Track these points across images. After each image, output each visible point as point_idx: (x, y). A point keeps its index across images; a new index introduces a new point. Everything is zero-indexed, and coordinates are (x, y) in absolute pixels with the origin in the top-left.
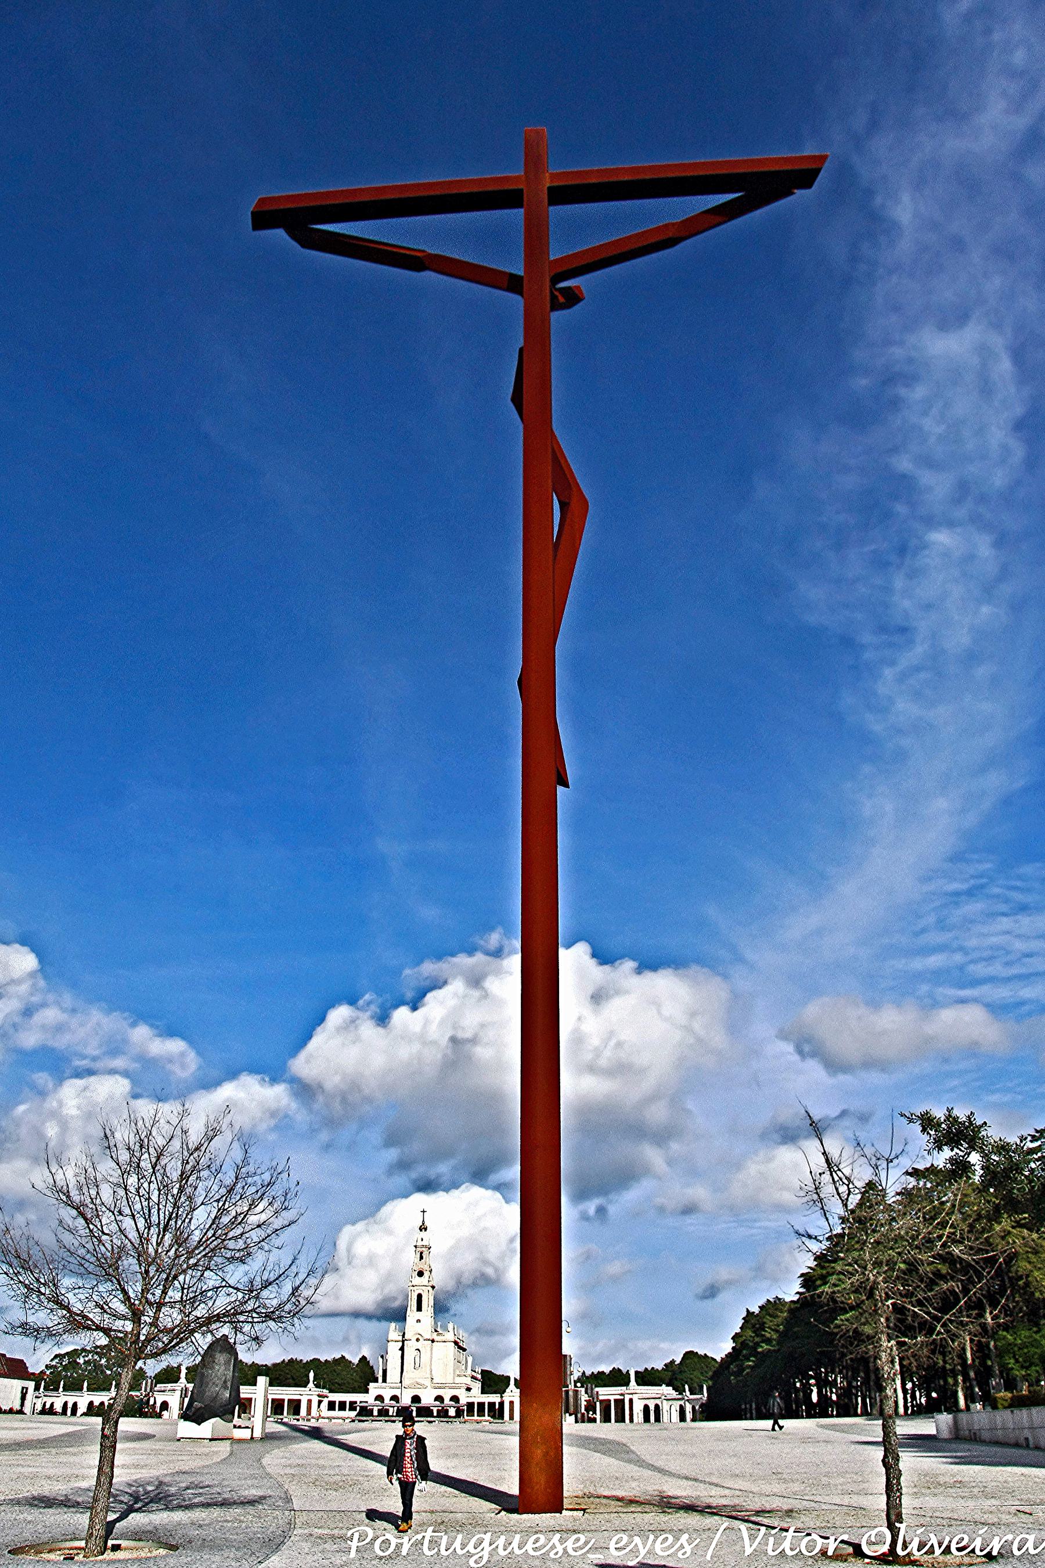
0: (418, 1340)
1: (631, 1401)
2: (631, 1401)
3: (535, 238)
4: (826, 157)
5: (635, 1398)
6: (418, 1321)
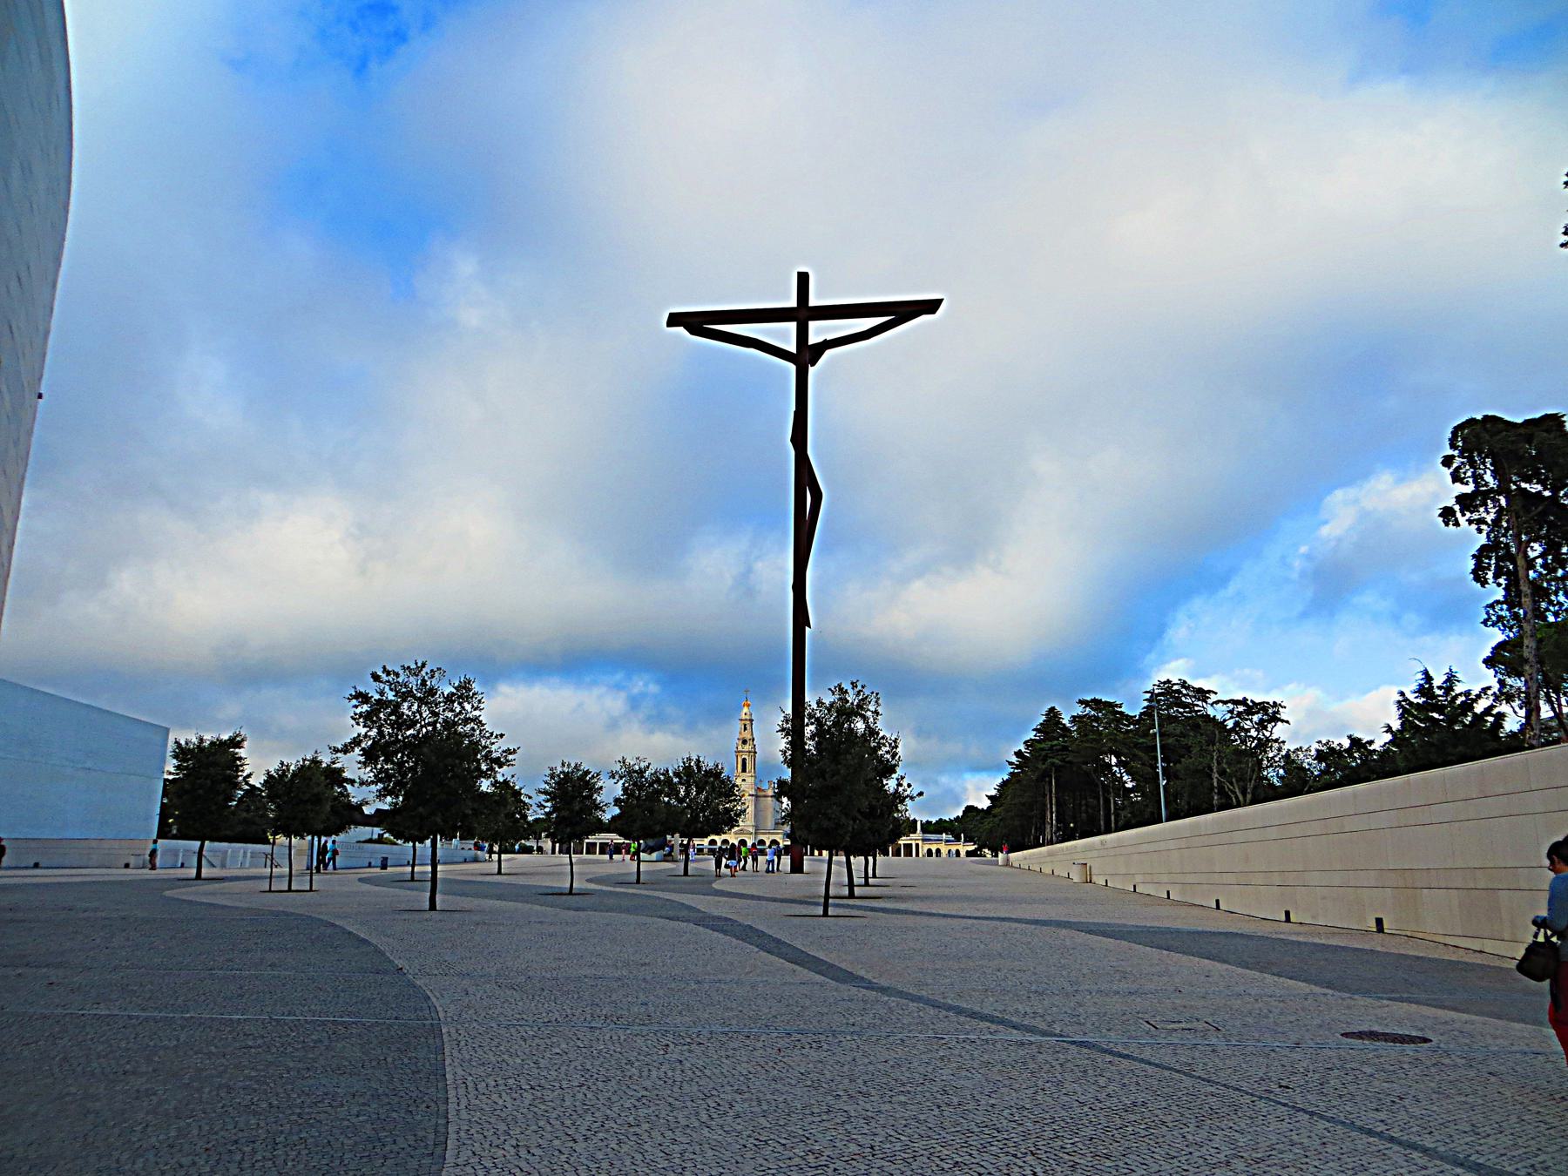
4: (938, 302)
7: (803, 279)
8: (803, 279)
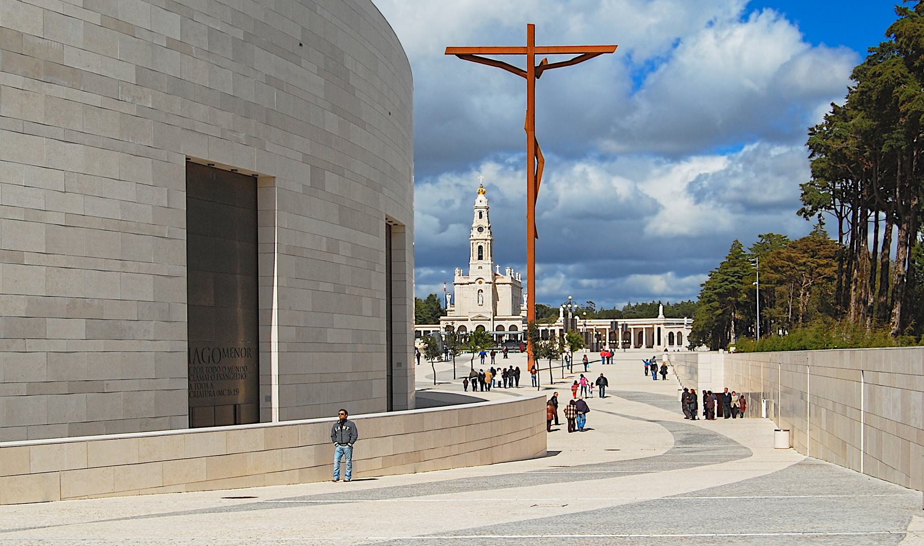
0: (480, 283)
1: (659, 329)
2: (659, 329)
3: (531, 60)
5: (662, 327)
6: (480, 267)
7: (531, 28)
8: (531, 28)
